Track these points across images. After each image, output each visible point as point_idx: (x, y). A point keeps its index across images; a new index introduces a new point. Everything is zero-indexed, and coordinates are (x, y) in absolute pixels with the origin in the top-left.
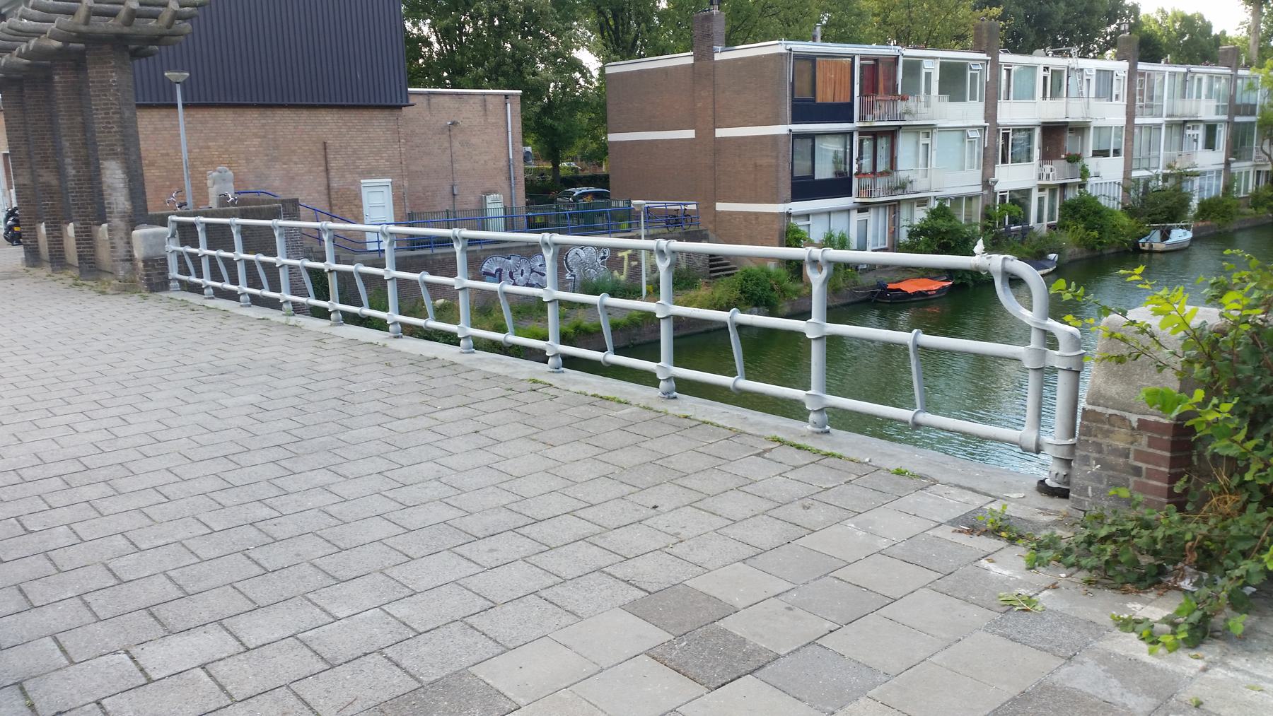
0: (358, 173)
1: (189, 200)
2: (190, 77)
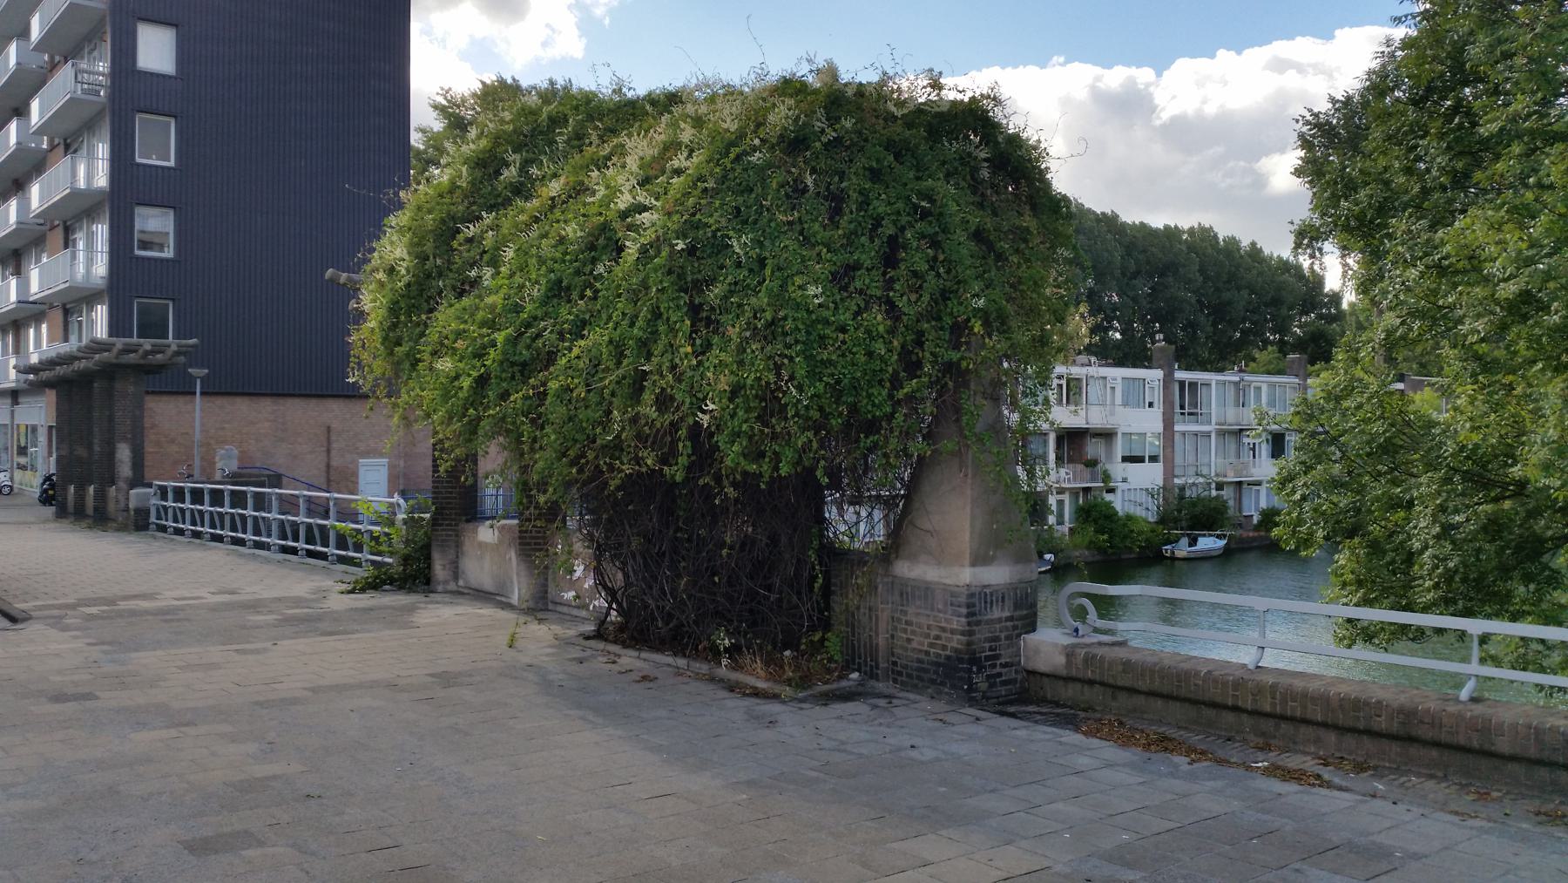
0: (358, 453)
1: (197, 473)
2: (208, 374)
